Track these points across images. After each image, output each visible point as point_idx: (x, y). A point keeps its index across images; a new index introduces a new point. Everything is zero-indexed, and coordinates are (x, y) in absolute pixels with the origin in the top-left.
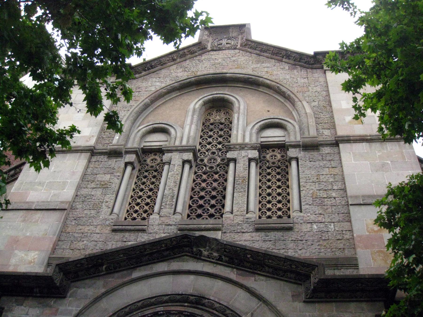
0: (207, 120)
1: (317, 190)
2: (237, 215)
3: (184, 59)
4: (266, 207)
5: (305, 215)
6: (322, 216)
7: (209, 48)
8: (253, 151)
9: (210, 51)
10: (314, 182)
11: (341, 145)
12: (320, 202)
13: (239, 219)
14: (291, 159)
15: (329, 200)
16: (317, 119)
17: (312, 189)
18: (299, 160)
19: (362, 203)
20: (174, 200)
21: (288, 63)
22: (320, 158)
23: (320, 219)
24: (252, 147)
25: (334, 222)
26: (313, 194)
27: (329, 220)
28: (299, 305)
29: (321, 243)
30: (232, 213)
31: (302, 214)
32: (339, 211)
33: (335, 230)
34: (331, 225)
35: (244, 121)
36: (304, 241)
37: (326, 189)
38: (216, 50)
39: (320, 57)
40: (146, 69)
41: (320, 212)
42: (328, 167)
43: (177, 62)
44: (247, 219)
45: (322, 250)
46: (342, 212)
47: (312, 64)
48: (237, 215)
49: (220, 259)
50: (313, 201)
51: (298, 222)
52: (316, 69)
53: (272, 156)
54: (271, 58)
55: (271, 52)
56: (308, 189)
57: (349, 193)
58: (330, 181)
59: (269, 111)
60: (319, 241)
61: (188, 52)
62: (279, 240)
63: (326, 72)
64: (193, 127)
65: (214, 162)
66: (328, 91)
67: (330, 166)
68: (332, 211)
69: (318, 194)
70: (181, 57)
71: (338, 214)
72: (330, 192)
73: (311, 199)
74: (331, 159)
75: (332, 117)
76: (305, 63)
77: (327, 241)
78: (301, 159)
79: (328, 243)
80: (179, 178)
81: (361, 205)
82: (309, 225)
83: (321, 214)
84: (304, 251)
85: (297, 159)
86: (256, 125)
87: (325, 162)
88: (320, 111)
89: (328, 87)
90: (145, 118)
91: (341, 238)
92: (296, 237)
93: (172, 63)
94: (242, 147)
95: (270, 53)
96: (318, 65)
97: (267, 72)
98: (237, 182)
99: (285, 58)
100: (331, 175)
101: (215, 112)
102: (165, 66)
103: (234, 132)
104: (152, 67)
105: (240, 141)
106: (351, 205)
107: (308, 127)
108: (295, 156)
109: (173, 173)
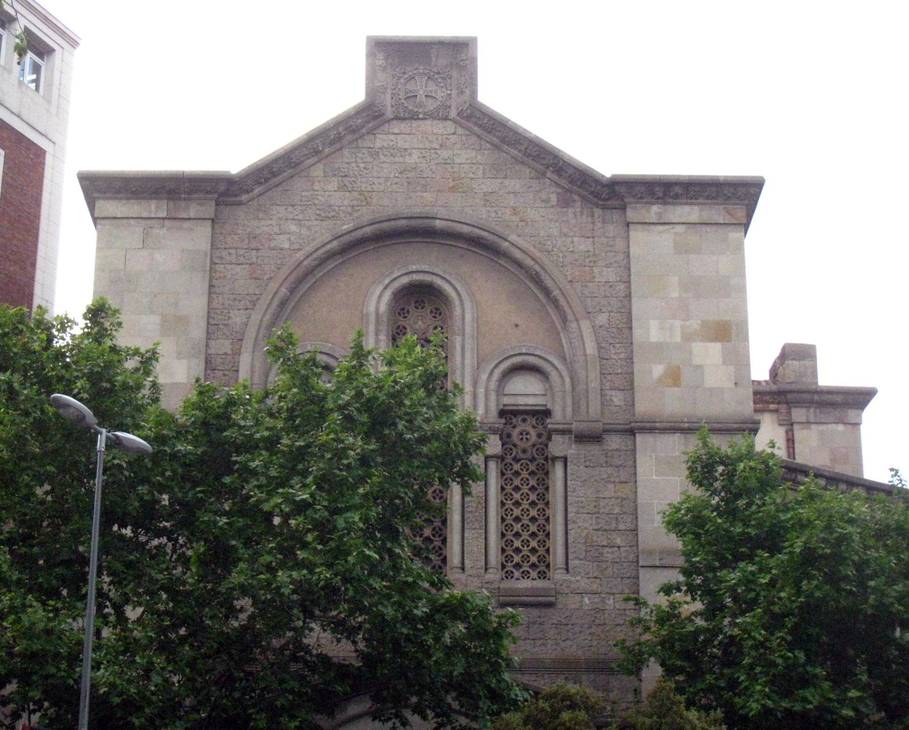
1: (594, 530)
2: (471, 576)
3: (337, 146)
4: (512, 546)
5: (573, 579)
6: (598, 580)
7: (389, 114)
9: (392, 119)
10: (589, 513)
11: (639, 438)
12: (596, 554)
14: (554, 459)
15: (610, 550)
16: (605, 361)
17: (586, 528)
18: (568, 464)
19: (658, 564)
21: (558, 185)
22: (602, 459)
23: (595, 586)
24: (490, 428)
25: (614, 594)
26: (587, 537)
27: (608, 590)
29: (593, 630)
30: (463, 569)
31: (568, 577)
32: (623, 574)
33: (615, 607)
34: (609, 599)
35: (473, 357)
36: (570, 626)
37: (608, 527)
38: (404, 119)
39: (622, 190)
40: (263, 180)
41: (596, 574)
42: (614, 482)
43: (323, 155)
44: (487, 583)
45: (595, 643)
46: (628, 575)
47: (604, 200)
48: (471, 576)
50: (586, 551)
51: (562, 591)
52: (611, 208)
53: (521, 434)
54: (523, 163)
55: (523, 148)
56: (579, 527)
57: (641, 547)
58: (615, 512)
59: (517, 326)
60: (590, 627)
61: (346, 129)
62: (534, 623)
63: (631, 227)
66: (629, 282)
67: (617, 480)
68: (613, 573)
69: (595, 538)
70: (331, 144)
71: (622, 578)
72: (614, 535)
73: (584, 548)
74: (620, 463)
75: (630, 360)
76: (592, 193)
77: (601, 627)
78: (572, 462)
79: (603, 632)
81: (656, 567)
82: (578, 598)
83: (596, 578)
84: (569, 643)
85: (565, 460)
86: (496, 371)
87: (610, 470)
88: (611, 341)
89: (635, 467)
91: (621, 622)
92: (558, 619)
93: (315, 159)
95: (520, 151)
96: (617, 203)
97: (514, 209)
98: (468, 507)
99: (552, 172)
100: (617, 498)
101: (413, 304)
102: (302, 167)
104: (274, 175)
106: (643, 567)
107: (587, 391)
108: (561, 454)
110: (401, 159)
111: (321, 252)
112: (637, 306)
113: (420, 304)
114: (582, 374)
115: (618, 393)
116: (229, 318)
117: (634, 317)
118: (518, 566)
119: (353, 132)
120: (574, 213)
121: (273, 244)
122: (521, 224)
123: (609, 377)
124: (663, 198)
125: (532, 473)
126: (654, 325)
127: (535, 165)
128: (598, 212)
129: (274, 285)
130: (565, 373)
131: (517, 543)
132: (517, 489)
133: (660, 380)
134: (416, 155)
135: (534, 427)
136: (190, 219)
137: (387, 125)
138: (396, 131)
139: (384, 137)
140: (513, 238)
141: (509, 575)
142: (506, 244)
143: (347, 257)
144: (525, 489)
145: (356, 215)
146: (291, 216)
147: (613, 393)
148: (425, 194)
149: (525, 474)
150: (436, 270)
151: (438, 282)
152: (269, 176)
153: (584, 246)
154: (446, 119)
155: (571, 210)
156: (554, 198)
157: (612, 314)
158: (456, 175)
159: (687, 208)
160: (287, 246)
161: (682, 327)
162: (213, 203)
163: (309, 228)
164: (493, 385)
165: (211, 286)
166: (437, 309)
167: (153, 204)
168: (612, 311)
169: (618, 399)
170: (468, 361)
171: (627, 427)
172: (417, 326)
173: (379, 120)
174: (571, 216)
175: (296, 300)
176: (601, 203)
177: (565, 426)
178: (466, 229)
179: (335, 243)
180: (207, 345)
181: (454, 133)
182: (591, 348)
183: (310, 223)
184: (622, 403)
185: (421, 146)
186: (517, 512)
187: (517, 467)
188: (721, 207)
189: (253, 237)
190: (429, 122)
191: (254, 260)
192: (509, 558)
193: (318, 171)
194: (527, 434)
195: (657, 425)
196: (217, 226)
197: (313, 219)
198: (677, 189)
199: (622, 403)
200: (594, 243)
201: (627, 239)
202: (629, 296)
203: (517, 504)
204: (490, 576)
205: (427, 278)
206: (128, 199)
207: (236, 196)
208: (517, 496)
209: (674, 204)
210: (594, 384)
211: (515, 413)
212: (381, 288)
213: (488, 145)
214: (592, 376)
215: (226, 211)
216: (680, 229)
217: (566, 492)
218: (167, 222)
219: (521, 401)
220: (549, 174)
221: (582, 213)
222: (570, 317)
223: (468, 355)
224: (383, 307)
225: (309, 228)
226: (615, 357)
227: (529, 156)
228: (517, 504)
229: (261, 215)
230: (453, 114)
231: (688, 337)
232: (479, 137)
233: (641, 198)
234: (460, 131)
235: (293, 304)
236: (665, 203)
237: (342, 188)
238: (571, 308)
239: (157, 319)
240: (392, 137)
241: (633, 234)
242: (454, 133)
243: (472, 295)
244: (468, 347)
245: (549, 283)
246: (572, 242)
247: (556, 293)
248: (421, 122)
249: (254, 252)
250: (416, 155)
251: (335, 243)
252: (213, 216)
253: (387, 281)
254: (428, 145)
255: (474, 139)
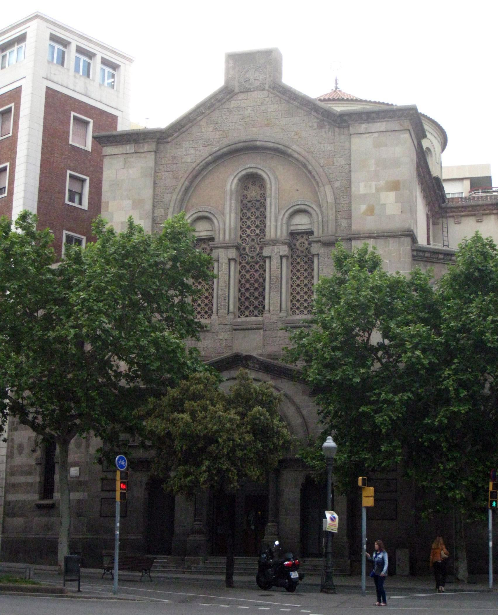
0: (245, 196)
3: (212, 109)
8: (284, 247)
13: (275, 318)
20: (227, 301)
21: (317, 118)
28: (306, 398)
30: (269, 311)
35: (275, 208)
39: (346, 118)
40: (177, 130)
49: (260, 369)
59: (297, 190)
61: (215, 100)
64: (233, 215)
65: (254, 251)
80: (227, 277)
85: (318, 255)
90: (188, 201)
94: (275, 242)
95: (298, 103)
97: (296, 132)
103: (267, 230)
104: (183, 127)
105: (273, 236)
108: (316, 253)
109: (222, 272)
110: (242, 113)
111: (203, 162)
112: (354, 177)
113: (254, 183)
114: (325, 212)
115: (344, 220)
116: (163, 198)
117: (352, 182)
118: (298, 308)
119: (219, 101)
120: (325, 132)
121: (183, 160)
122: (299, 139)
123: (340, 213)
124: (367, 120)
125: (306, 263)
126: (362, 185)
127: (305, 108)
128: (336, 129)
129: (182, 181)
130: (319, 212)
131: (298, 297)
132: (298, 271)
133: (365, 213)
134: (250, 109)
135: (298, 240)
136: (144, 152)
137: (236, 96)
138: (240, 98)
139: (235, 102)
140: (294, 147)
141: (294, 313)
142: (290, 151)
143: (217, 164)
144: (302, 271)
145: (221, 142)
146: (191, 146)
147: (342, 220)
148: (253, 129)
149: (302, 263)
150: (259, 166)
151: (260, 172)
152: (180, 127)
153: (329, 147)
154: (264, 90)
155: (323, 130)
156: (315, 125)
157: (343, 181)
158: (269, 118)
159: (379, 124)
160: (189, 161)
161: (376, 185)
162: (155, 143)
163: (200, 151)
164: (285, 220)
165: (155, 183)
166: (262, 185)
167: (128, 147)
168: (342, 180)
169: (344, 223)
170: (273, 210)
171: (347, 237)
172: (252, 194)
173: (232, 94)
174: (323, 133)
175: (195, 186)
176: (337, 125)
177: (318, 239)
178: (271, 145)
179: (210, 157)
180: (153, 212)
181: (268, 97)
182: (330, 199)
183: (200, 148)
184: (346, 225)
185: (252, 105)
186: (298, 282)
187: (298, 260)
188: (397, 122)
189: (174, 158)
190: (256, 92)
191: (175, 169)
192: (294, 305)
193: (203, 123)
194: (254, 248)
195: (361, 235)
196: (158, 154)
197: (201, 146)
198: (374, 115)
199: (346, 225)
200: (334, 146)
201: (350, 142)
202: (350, 171)
203: (298, 278)
204: (283, 314)
205: (254, 171)
206: (117, 145)
207: (165, 139)
208: (298, 274)
209: (373, 122)
210: (332, 217)
211: (298, 234)
212: (233, 177)
213: (284, 101)
214: (330, 212)
215: (161, 147)
216: (376, 135)
217: (319, 271)
218: (134, 155)
219: (300, 227)
220: (313, 113)
221: (329, 131)
222: (320, 184)
223: (273, 207)
224: (233, 187)
225: (200, 151)
226: (343, 202)
227: (302, 105)
228: (298, 278)
229: (178, 147)
230: (267, 87)
231: (378, 190)
232: (279, 97)
233: (356, 121)
234: (271, 95)
235: (193, 189)
236: (368, 123)
237: (215, 130)
238: (321, 180)
239: (130, 202)
240: (238, 102)
241: (352, 139)
242: (268, 97)
243: (276, 178)
244: (273, 204)
245: (310, 168)
246: (324, 146)
247: (314, 173)
248: (251, 93)
249: (175, 165)
250: (250, 109)
251: (210, 157)
252: (155, 150)
253: (235, 174)
254: (255, 104)
255: (277, 98)
